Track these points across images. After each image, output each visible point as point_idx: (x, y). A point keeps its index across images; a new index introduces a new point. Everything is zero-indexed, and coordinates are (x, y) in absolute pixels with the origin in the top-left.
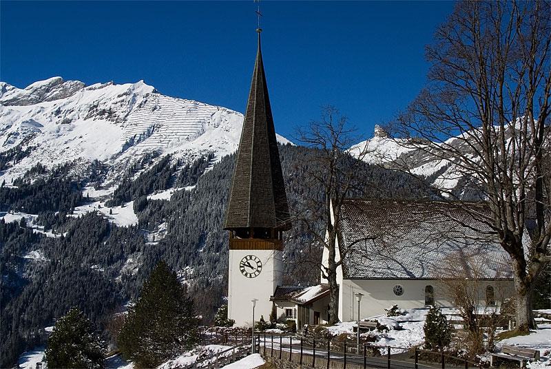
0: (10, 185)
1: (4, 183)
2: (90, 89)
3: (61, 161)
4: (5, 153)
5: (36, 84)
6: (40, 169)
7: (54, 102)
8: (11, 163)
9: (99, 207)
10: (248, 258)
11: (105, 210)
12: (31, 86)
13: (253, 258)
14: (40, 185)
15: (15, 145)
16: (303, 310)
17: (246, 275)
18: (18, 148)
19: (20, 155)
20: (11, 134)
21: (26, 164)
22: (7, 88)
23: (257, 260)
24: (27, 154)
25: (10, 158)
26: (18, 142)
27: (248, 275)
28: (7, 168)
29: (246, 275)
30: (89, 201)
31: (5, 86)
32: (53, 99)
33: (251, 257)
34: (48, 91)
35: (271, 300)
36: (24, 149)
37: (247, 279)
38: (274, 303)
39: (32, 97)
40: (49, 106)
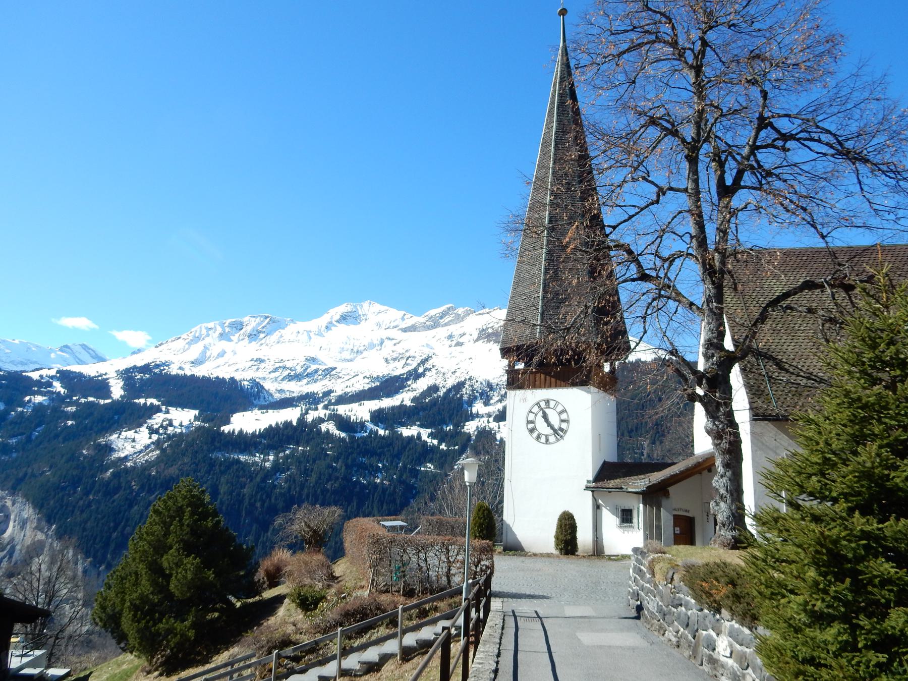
0: (408, 403)
1: (402, 401)
2: (480, 314)
3: (451, 382)
4: (404, 374)
5: (433, 312)
6: (434, 388)
7: (446, 328)
8: (409, 383)
9: (488, 422)
10: (543, 404)
11: (493, 425)
12: (427, 314)
13: (552, 404)
14: (434, 403)
15: (413, 367)
16: (651, 512)
17: (538, 438)
18: (416, 370)
19: (416, 375)
20: (409, 357)
21: (421, 385)
22: (405, 317)
23: (559, 409)
24: (423, 375)
25: (407, 379)
26: (414, 365)
27: (543, 439)
28: (405, 387)
29: (538, 438)
30: (477, 415)
31: (404, 315)
32: (446, 325)
33: (547, 402)
34: (441, 318)
35: (587, 488)
36: (421, 370)
37: (541, 447)
38: (595, 499)
39: (428, 323)
40: (441, 332)
